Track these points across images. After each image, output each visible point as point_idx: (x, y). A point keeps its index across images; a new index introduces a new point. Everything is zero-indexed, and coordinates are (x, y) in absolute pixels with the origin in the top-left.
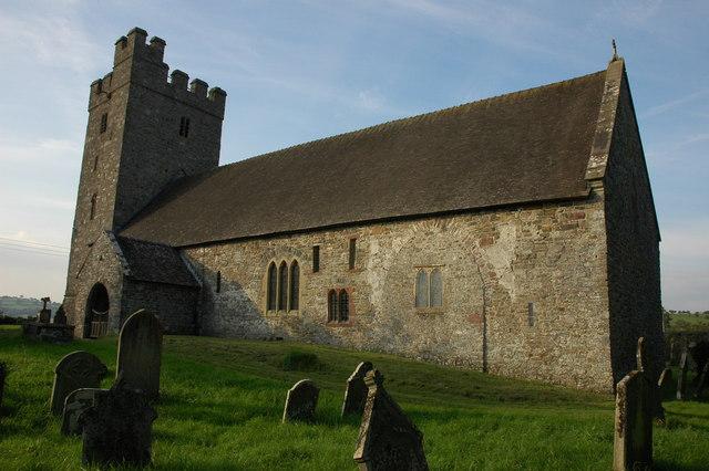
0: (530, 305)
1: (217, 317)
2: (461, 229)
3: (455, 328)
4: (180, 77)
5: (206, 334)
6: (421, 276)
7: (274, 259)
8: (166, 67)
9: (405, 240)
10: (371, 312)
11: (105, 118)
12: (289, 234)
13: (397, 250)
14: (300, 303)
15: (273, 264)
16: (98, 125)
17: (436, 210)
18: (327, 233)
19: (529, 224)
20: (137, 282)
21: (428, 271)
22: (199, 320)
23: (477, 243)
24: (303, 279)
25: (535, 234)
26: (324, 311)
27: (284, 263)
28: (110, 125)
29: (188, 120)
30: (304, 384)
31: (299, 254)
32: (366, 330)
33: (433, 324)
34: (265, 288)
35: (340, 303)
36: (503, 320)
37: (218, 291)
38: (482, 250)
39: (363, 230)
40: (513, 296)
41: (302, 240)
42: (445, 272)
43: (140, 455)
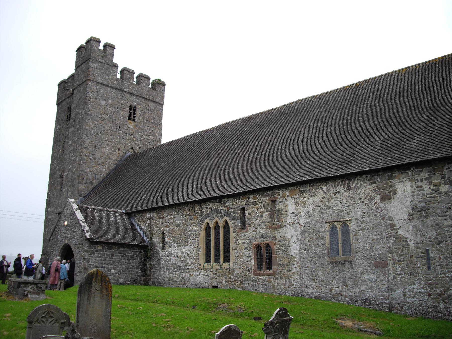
0: (427, 250)
1: (163, 270)
2: (365, 189)
3: (362, 274)
4: (127, 72)
5: (154, 284)
6: (333, 230)
7: (208, 220)
8: (116, 66)
9: (317, 199)
10: (290, 259)
11: (69, 109)
12: (219, 199)
13: (311, 208)
14: (231, 256)
15: (208, 224)
16: (64, 117)
17: (341, 172)
18: (251, 196)
19: (421, 180)
20: (97, 243)
21: (338, 226)
22: (148, 272)
23: (378, 198)
24: (232, 235)
25: (427, 188)
26: (252, 263)
27: (217, 226)
28: (73, 115)
29: (135, 107)
30: (229, 329)
31: (228, 215)
32: (288, 278)
33: (343, 270)
34: (202, 245)
35: (265, 255)
36: (404, 265)
37: (163, 248)
38: (382, 205)
39: (281, 192)
40: (411, 244)
41: (232, 204)
42: (352, 226)
43: (286, 332)
